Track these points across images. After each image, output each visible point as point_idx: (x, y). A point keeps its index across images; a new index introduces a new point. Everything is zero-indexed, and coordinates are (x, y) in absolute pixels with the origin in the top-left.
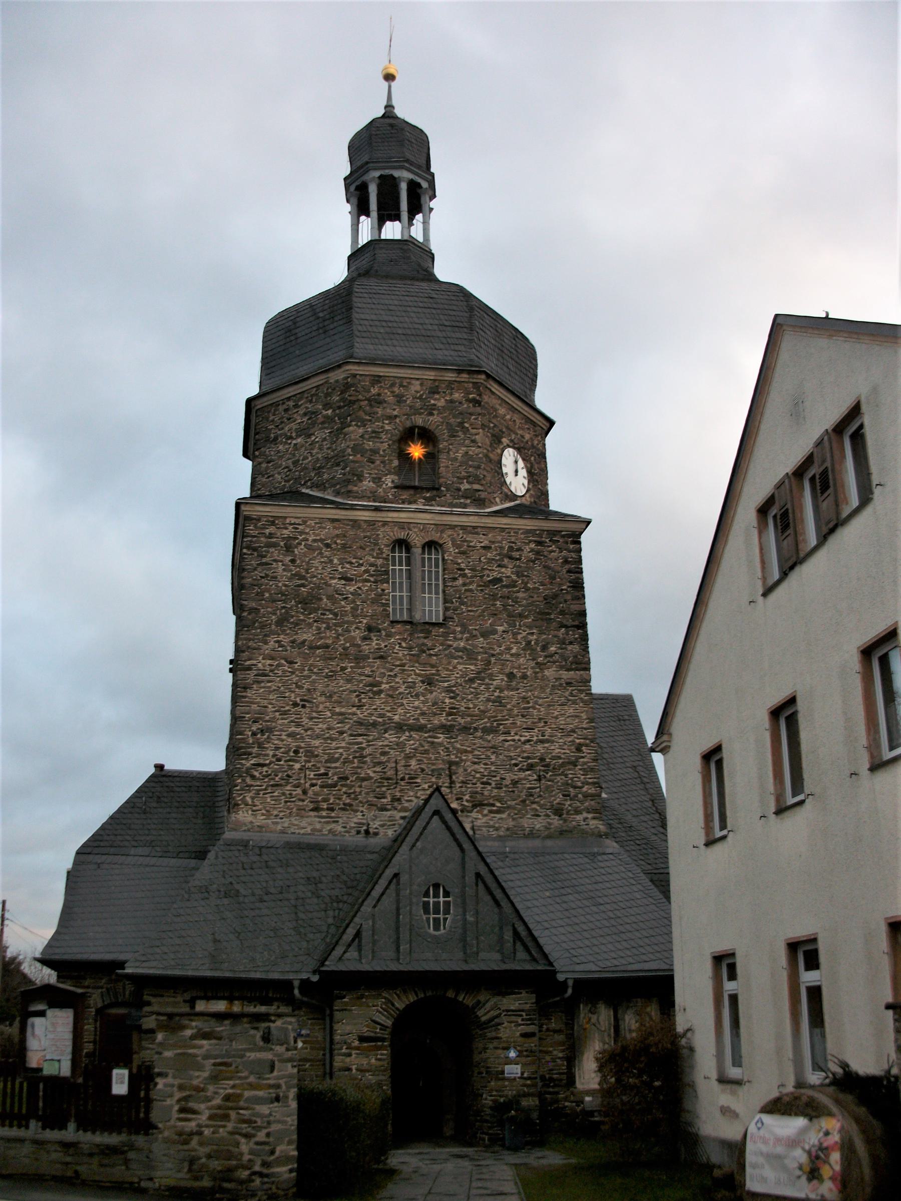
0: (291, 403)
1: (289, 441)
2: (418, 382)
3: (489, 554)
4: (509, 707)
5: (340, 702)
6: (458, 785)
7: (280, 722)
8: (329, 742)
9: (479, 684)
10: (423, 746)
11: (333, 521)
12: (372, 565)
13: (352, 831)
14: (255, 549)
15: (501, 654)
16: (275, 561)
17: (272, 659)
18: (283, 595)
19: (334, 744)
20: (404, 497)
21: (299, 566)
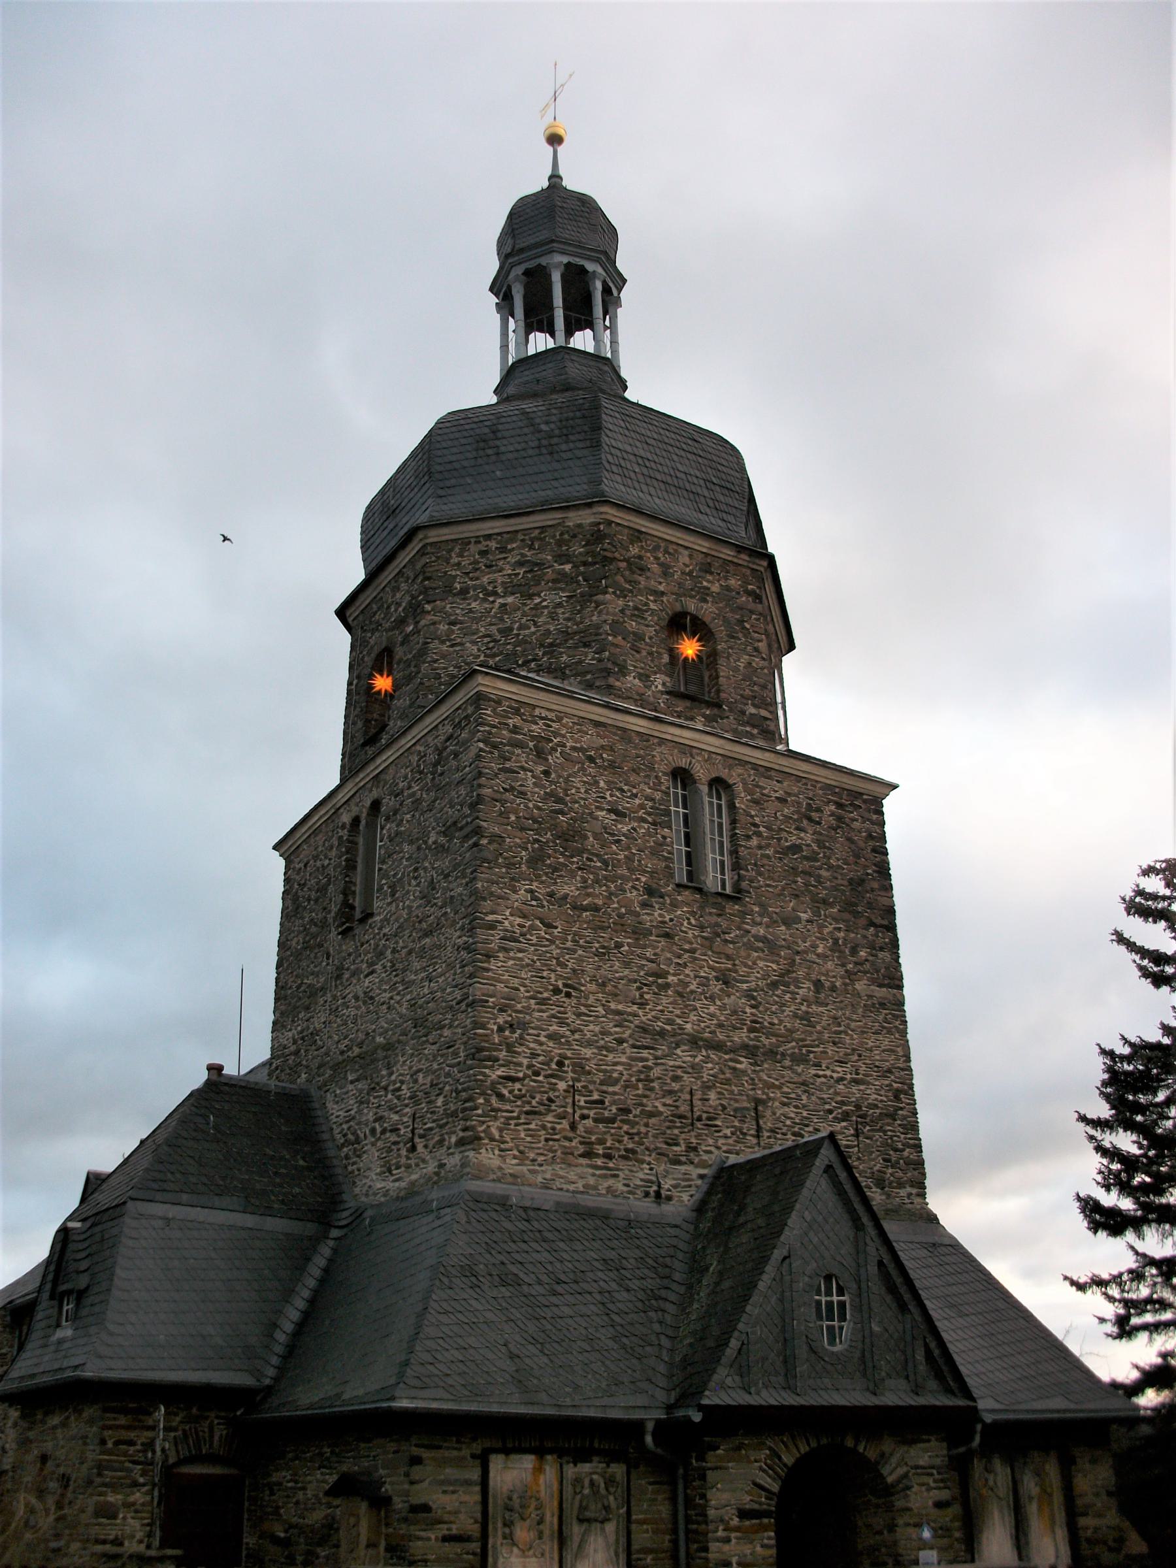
0: (493, 545)
1: (491, 599)
2: (686, 553)
3: (786, 810)
4: (818, 1028)
5: (616, 995)
6: (766, 1134)
7: (536, 1014)
8: (605, 1053)
9: (783, 991)
10: (724, 1073)
11: (597, 724)
12: (648, 798)
13: (638, 1192)
14: (495, 746)
15: (806, 952)
16: (523, 768)
17: (524, 917)
18: (535, 821)
19: (611, 1057)
20: (678, 709)
21: (555, 783)
